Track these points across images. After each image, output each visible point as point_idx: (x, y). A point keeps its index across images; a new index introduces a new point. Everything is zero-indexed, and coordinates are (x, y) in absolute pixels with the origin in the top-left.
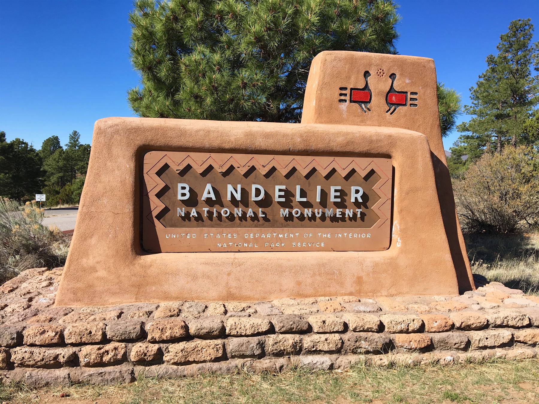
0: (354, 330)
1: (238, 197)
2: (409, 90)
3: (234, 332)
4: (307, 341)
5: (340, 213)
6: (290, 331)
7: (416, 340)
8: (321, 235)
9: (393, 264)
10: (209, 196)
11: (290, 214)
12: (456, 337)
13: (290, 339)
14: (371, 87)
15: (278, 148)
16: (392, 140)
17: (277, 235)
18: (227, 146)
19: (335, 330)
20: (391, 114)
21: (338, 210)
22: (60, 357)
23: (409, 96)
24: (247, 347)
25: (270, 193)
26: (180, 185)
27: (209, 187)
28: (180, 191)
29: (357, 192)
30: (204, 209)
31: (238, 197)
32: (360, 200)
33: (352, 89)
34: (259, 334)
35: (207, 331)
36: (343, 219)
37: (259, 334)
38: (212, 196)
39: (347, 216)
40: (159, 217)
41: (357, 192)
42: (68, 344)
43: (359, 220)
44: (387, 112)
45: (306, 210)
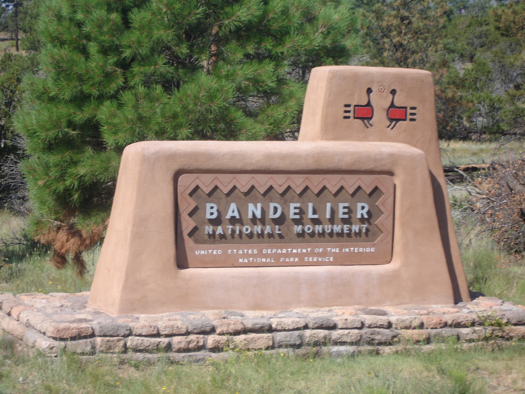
0: (369, 327)
1: (258, 215)
2: (409, 104)
3: (279, 328)
4: (335, 334)
5: (348, 229)
6: (321, 327)
7: (416, 333)
8: (331, 250)
9: (395, 276)
10: (233, 215)
11: (303, 231)
12: (447, 332)
13: (322, 333)
14: (373, 103)
15: (293, 168)
16: (394, 158)
17: (292, 251)
18: (249, 168)
19: (354, 326)
20: (392, 129)
21: (345, 226)
22: (161, 343)
23: (409, 111)
24: (291, 338)
25: (265, 209)
26: (209, 205)
27: (233, 206)
28: (208, 211)
29: (363, 208)
30: (228, 227)
31: (258, 215)
32: (366, 216)
33: (355, 106)
34: (298, 329)
35: (260, 326)
36: (349, 235)
37: (298, 329)
38: (236, 214)
39: (353, 231)
40: (190, 235)
41: (363, 208)
42: (163, 335)
43: (363, 235)
44: (388, 127)
45: (317, 226)
